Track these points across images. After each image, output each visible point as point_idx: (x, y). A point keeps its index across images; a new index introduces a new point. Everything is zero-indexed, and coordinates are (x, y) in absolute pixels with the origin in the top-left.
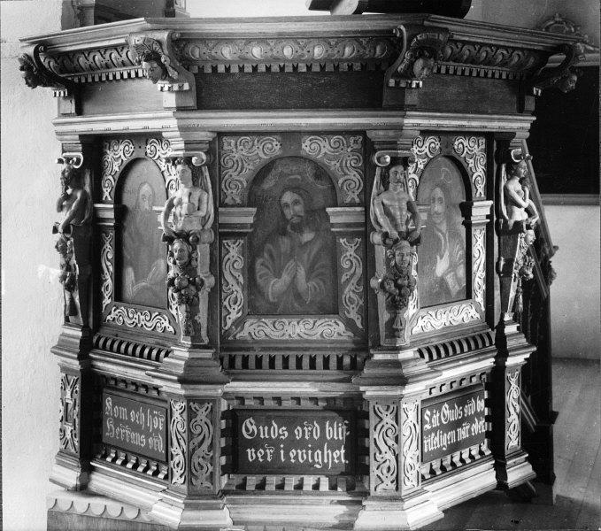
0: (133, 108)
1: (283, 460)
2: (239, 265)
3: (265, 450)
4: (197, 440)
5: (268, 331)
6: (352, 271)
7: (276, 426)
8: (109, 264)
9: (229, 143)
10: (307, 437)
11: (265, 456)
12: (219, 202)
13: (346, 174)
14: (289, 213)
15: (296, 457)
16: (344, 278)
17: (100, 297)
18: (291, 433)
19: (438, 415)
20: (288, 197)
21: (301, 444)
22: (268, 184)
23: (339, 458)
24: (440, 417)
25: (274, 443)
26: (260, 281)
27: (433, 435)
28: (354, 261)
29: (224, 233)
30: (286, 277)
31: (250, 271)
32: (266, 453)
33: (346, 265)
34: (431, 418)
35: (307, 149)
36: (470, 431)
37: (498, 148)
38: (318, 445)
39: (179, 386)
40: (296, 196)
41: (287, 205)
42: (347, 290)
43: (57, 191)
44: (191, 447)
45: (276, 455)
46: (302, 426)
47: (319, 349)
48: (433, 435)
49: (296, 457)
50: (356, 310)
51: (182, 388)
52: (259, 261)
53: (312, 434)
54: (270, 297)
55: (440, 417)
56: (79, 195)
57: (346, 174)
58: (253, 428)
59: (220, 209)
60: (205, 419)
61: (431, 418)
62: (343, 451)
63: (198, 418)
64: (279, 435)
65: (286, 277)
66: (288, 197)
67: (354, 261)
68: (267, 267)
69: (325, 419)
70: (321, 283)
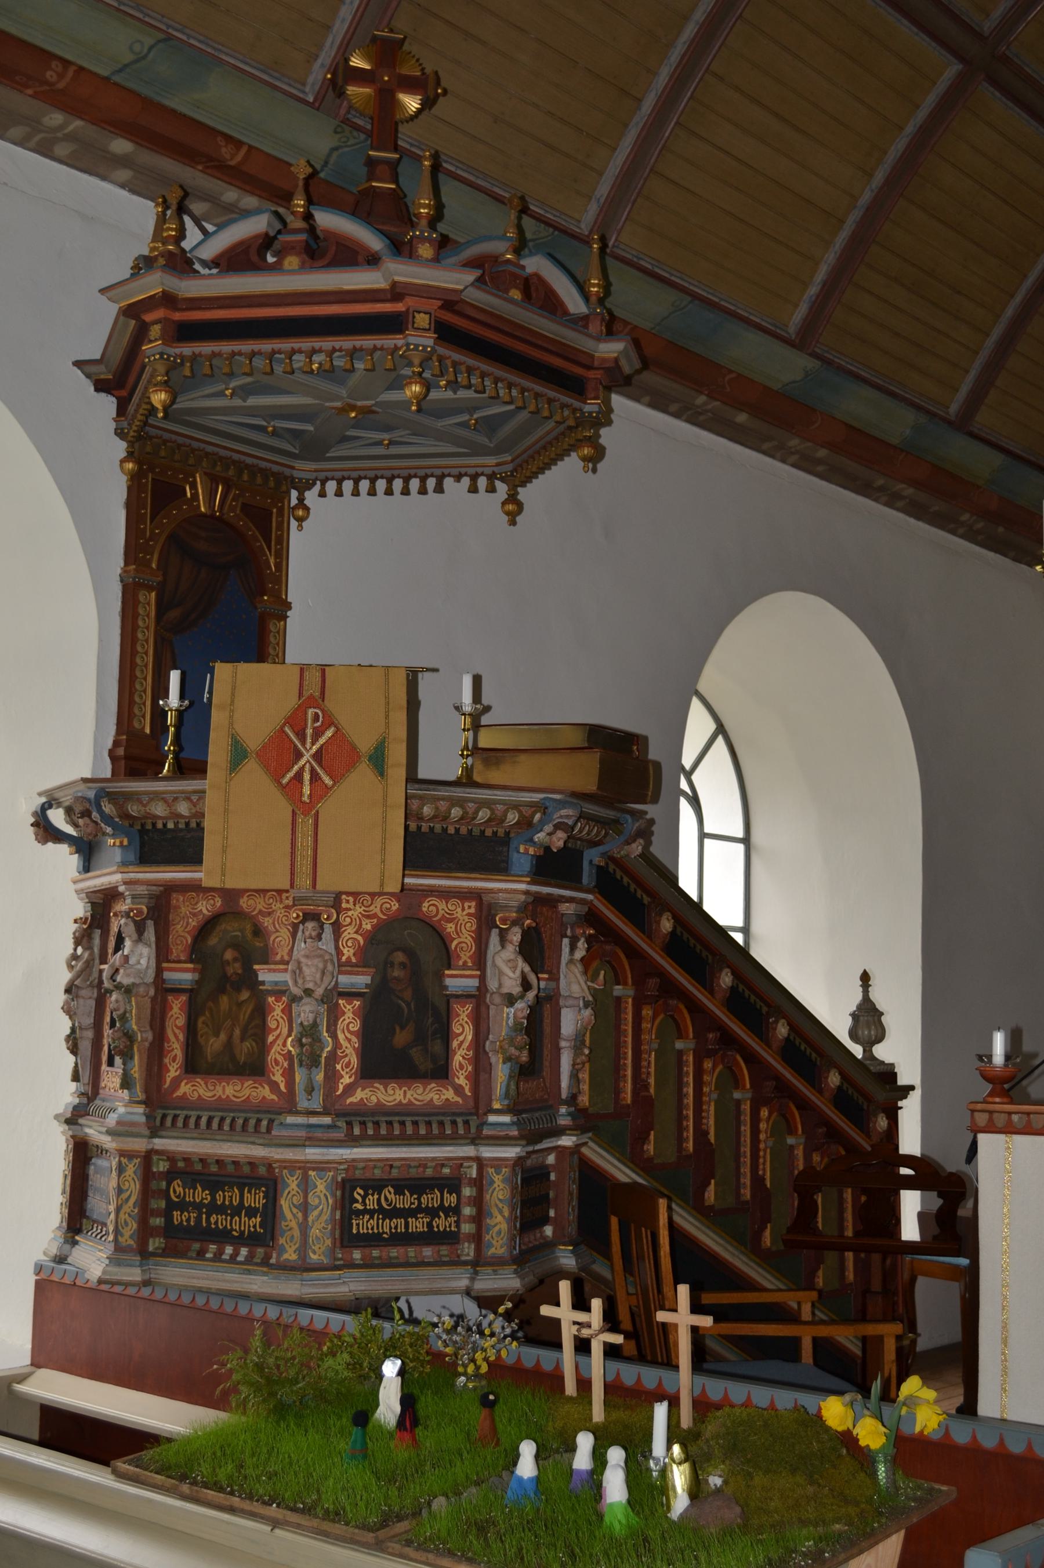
0: (523, 897)
1: (204, 1225)
2: (181, 1022)
3: (189, 1213)
4: (125, 1196)
5: (201, 1091)
6: (278, 1032)
7: (200, 1189)
8: (177, 1031)
9: (177, 899)
10: (227, 1203)
11: (188, 1220)
12: (162, 954)
13: (277, 931)
14: (230, 971)
15: (216, 1223)
16: (271, 1039)
17: (162, 1069)
18: (214, 1199)
19: (376, 1196)
20: (229, 955)
21: (221, 1210)
22: (213, 941)
23: (255, 1226)
24: (379, 1200)
25: (198, 1206)
26: (201, 1041)
27: (367, 1217)
28: (281, 1020)
29: (163, 990)
30: (223, 1036)
31: (191, 1029)
32: (190, 1217)
33: (272, 1025)
34: (364, 1198)
35: (244, 906)
36: (430, 1225)
37: (486, 917)
38: (237, 1211)
39: (109, 1138)
40: (236, 954)
41: (228, 962)
42: (273, 1050)
43: (67, 947)
44: (120, 1202)
45: (199, 1219)
46: (224, 1192)
47: (240, 1111)
48: (367, 1217)
49: (216, 1223)
50: (281, 1072)
51: (113, 1140)
52: (201, 1020)
53: (231, 1200)
54: (209, 1057)
55: (379, 1200)
56: (86, 955)
57: (277, 931)
58: (179, 1190)
59: (165, 965)
60: (133, 1175)
61: (364, 1198)
62: (259, 1219)
63: (127, 1174)
64: (203, 1199)
65: (223, 1036)
66: (229, 955)
67: (281, 1020)
68: (207, 1025)
69: (245, 1185)
70: (254, 1044)
